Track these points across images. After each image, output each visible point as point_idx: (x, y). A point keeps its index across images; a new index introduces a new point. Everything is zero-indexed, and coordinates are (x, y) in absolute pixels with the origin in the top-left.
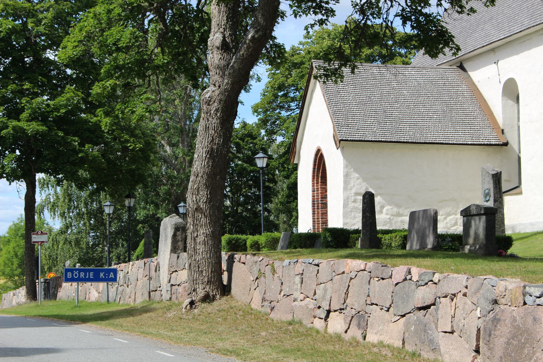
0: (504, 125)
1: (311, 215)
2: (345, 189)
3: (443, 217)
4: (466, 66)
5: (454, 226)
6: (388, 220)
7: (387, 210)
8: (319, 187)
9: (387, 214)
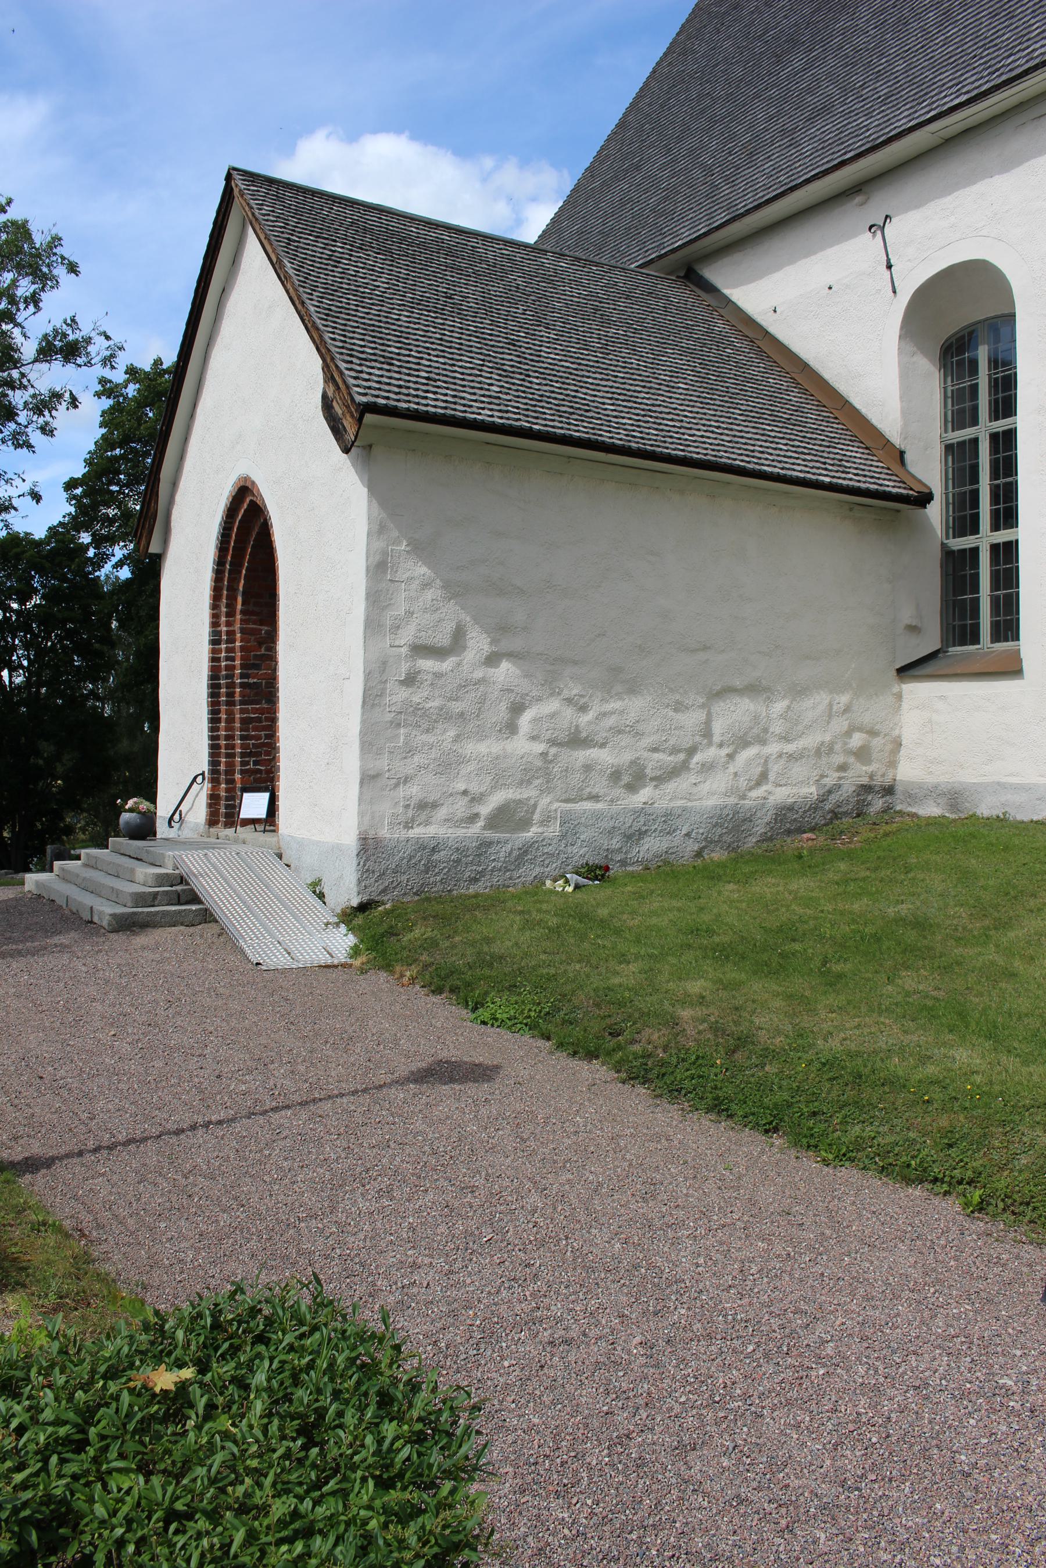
0: (905, 435)
1: (205, 725)
2: (373, 626)
3: (725, 751)
4: (712, 274)
5: (758, 784)
6: (539, 763)
7: (535, 720)
8: (237, 626)
9: (534, 738)
